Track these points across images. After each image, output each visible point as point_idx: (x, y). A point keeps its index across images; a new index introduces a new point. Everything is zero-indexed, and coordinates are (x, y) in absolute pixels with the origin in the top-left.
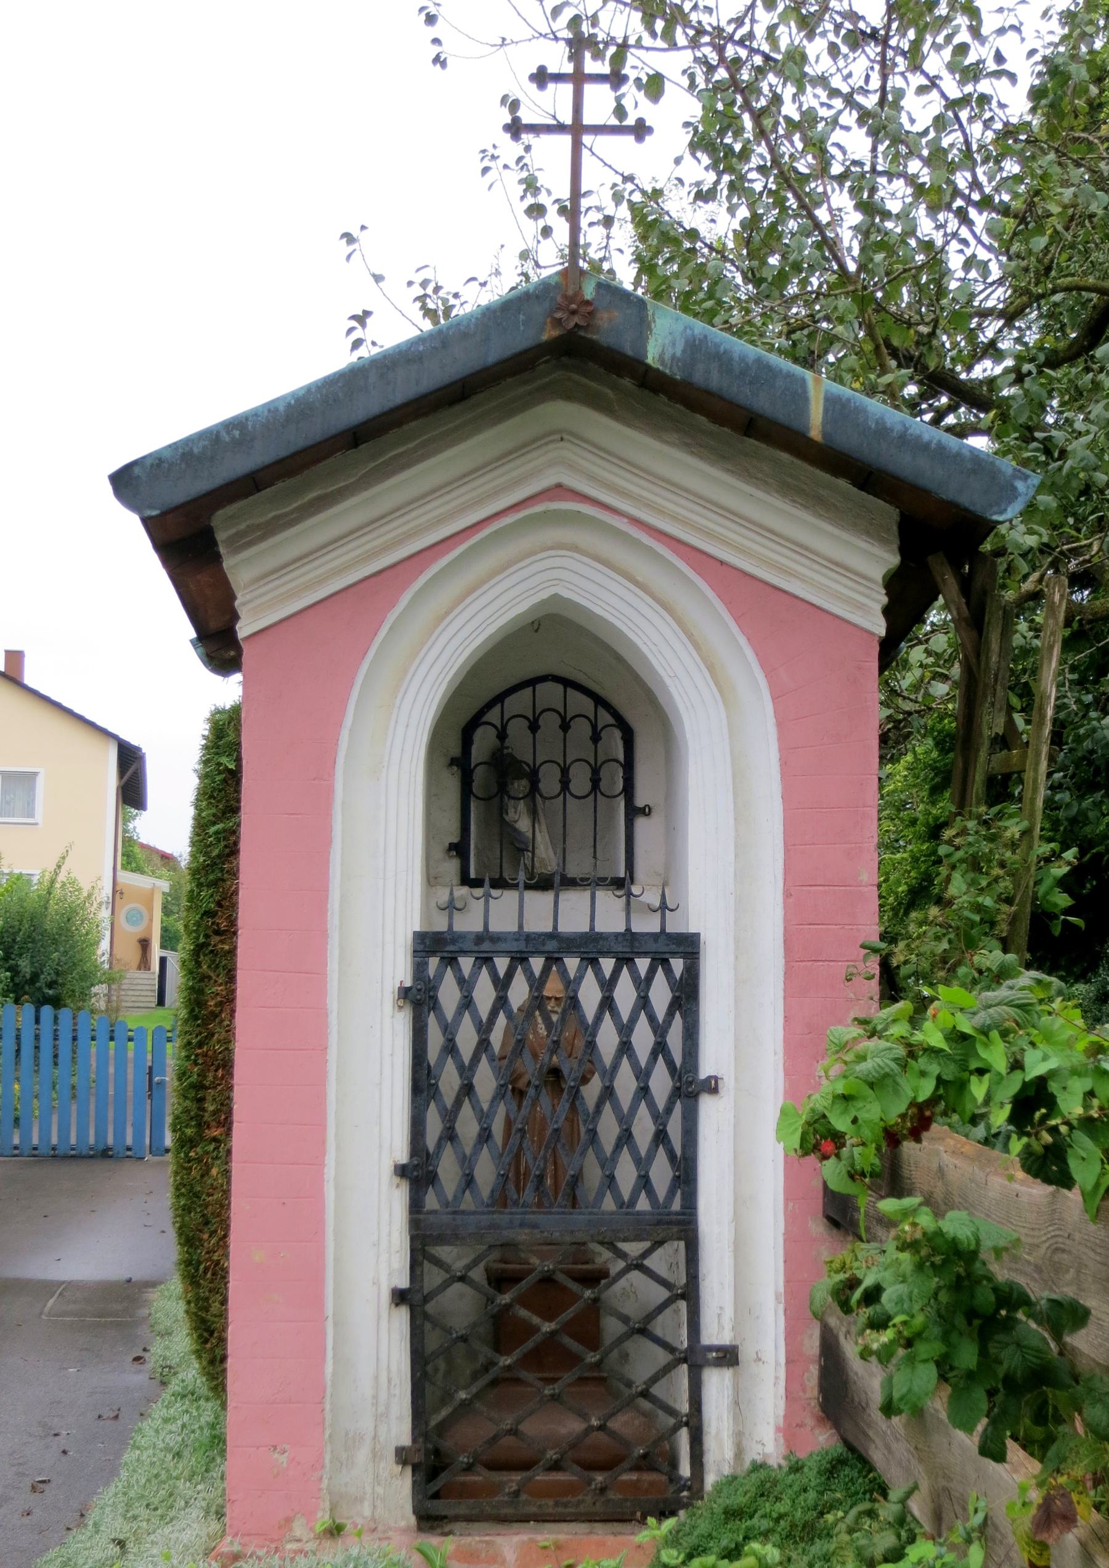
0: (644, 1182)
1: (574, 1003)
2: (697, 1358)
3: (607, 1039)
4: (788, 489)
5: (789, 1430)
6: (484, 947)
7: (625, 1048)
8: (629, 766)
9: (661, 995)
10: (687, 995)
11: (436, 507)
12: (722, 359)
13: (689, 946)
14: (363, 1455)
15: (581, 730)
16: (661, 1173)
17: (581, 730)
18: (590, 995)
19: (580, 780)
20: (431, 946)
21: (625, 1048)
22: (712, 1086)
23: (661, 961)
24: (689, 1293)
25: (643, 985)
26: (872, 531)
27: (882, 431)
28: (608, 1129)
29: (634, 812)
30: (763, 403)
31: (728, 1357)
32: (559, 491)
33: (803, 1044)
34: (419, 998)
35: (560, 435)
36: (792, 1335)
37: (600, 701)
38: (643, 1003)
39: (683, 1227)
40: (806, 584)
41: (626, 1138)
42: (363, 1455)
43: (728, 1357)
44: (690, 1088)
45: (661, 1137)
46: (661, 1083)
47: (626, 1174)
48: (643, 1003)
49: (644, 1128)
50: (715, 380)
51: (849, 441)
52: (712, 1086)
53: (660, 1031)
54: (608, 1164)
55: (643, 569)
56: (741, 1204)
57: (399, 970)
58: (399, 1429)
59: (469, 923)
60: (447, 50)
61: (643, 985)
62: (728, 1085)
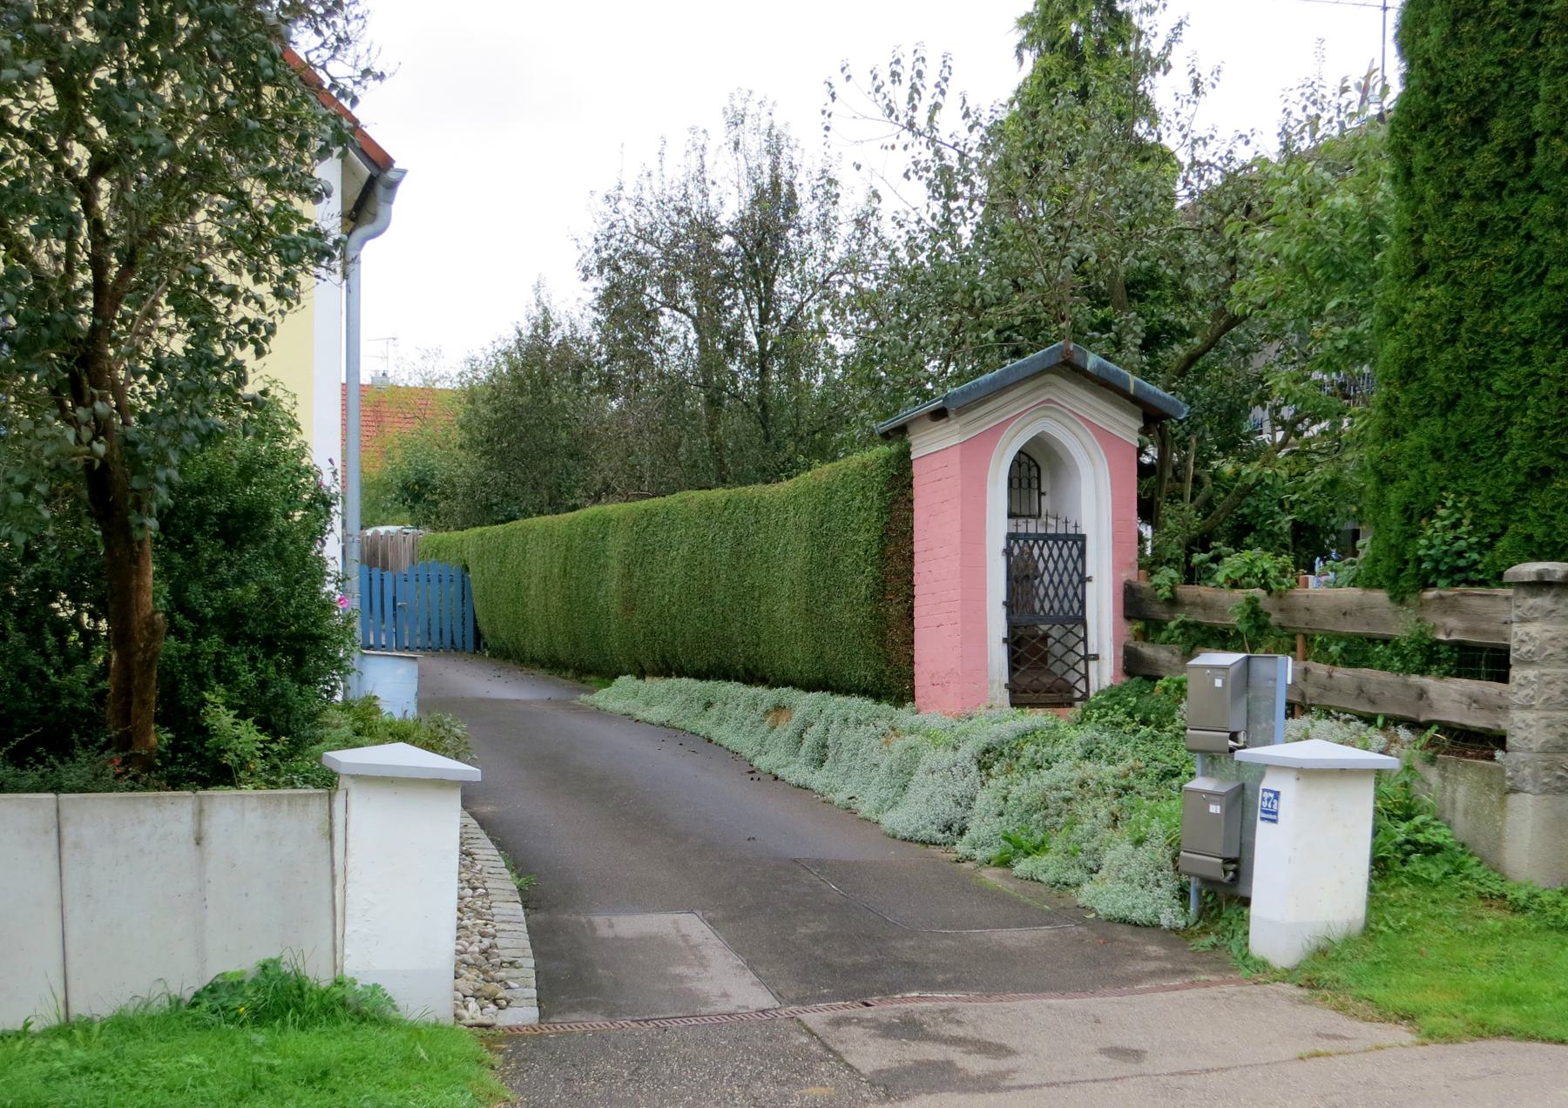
0: (1071, 607)
1: (1031, 554)
2: (1087, 658)
3: (1041, 565)
4: (1113, 403)
5: (1115, 677)
6: (1027, 537)
7: (1046, 568)
8: (1039, 479)
9: (1075, 552)
10: (1082, 553)
11: (1015, 405)
12: (1107, 369)
13: (1083, 538)
14: (996, 686)
15: (1025, 467)
16: (1076, 605)
17: (1025, 467)
18: (1036, 552)
19: (1025, 483)
20: (1012, 537)
21: (1046, 568)
22: (1089, 579)
23: (1075, 542)
24: (1085, 640)
25: (1070, 549)
26: (1133, 414)
27: (1149, 392)
28: (1042, 592)
29: (1041, 494)
30: (1117, 382)
31: (1096, 657)
32: (1049, 401)
33: (1118, 566)
34: (1008, 552)
35: (1050, 384)
36: (1115, 651)
37: (1030, 458)
38: (1070, 555)
39: (1082, 621)
40: (1117, 431)
41: (1046, 594)
42: (996, 686)
43: (1096, 657)
44: (1084, 580)
45: (1076, 594)
46: (1076, 579)
47: (1047, 605)
48: (1070, 555)
49: (1071, 592)
50: (1105, 375)
51: (1141, 395)
52: (1089, 579)
53: (1075, 563)
54: (1042, 602)
55: (1066, 421)
56: (1099, 614)
57: (1002, 544)
58: (1006, 679)
59: (1022, 530)
60: (832, 122)
61: (1070, 549)
62: (1095, 579)
